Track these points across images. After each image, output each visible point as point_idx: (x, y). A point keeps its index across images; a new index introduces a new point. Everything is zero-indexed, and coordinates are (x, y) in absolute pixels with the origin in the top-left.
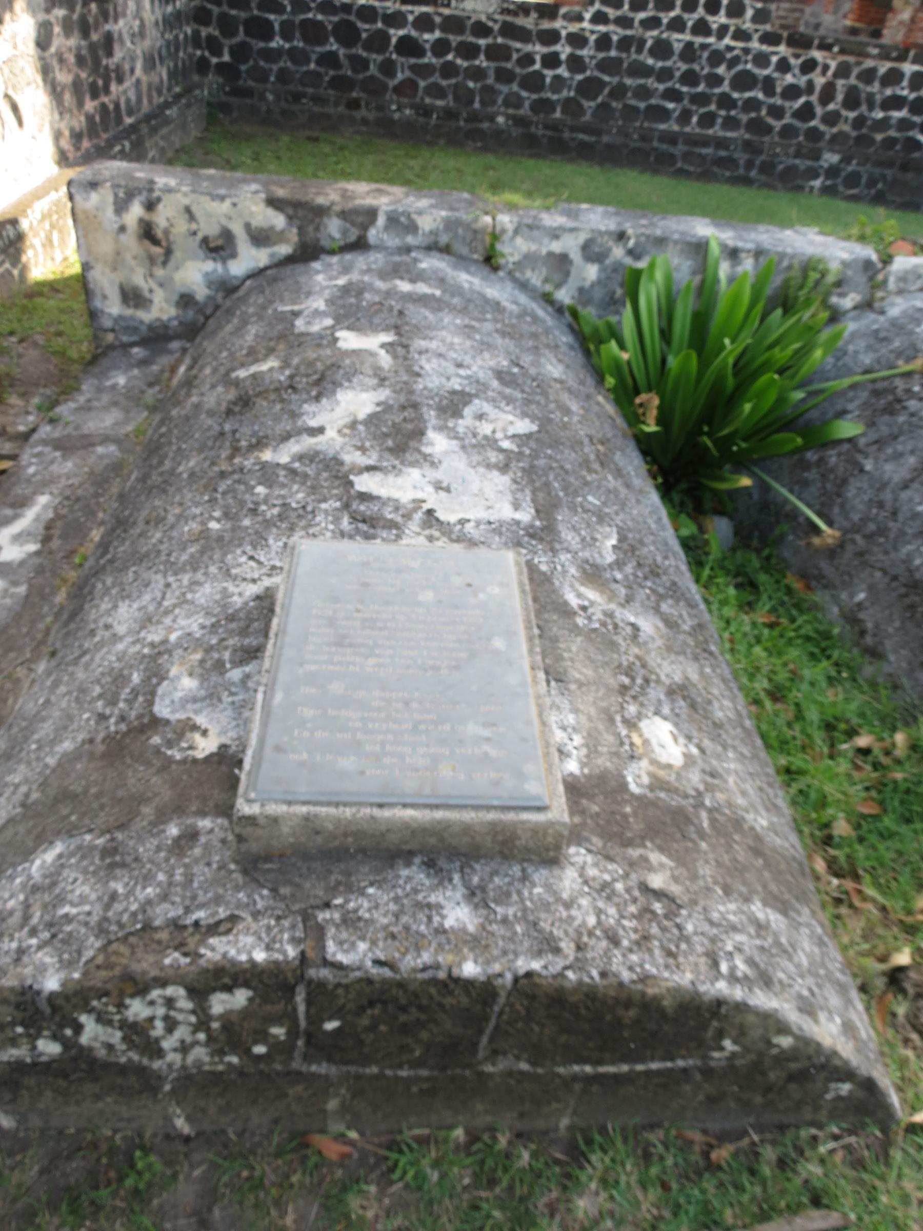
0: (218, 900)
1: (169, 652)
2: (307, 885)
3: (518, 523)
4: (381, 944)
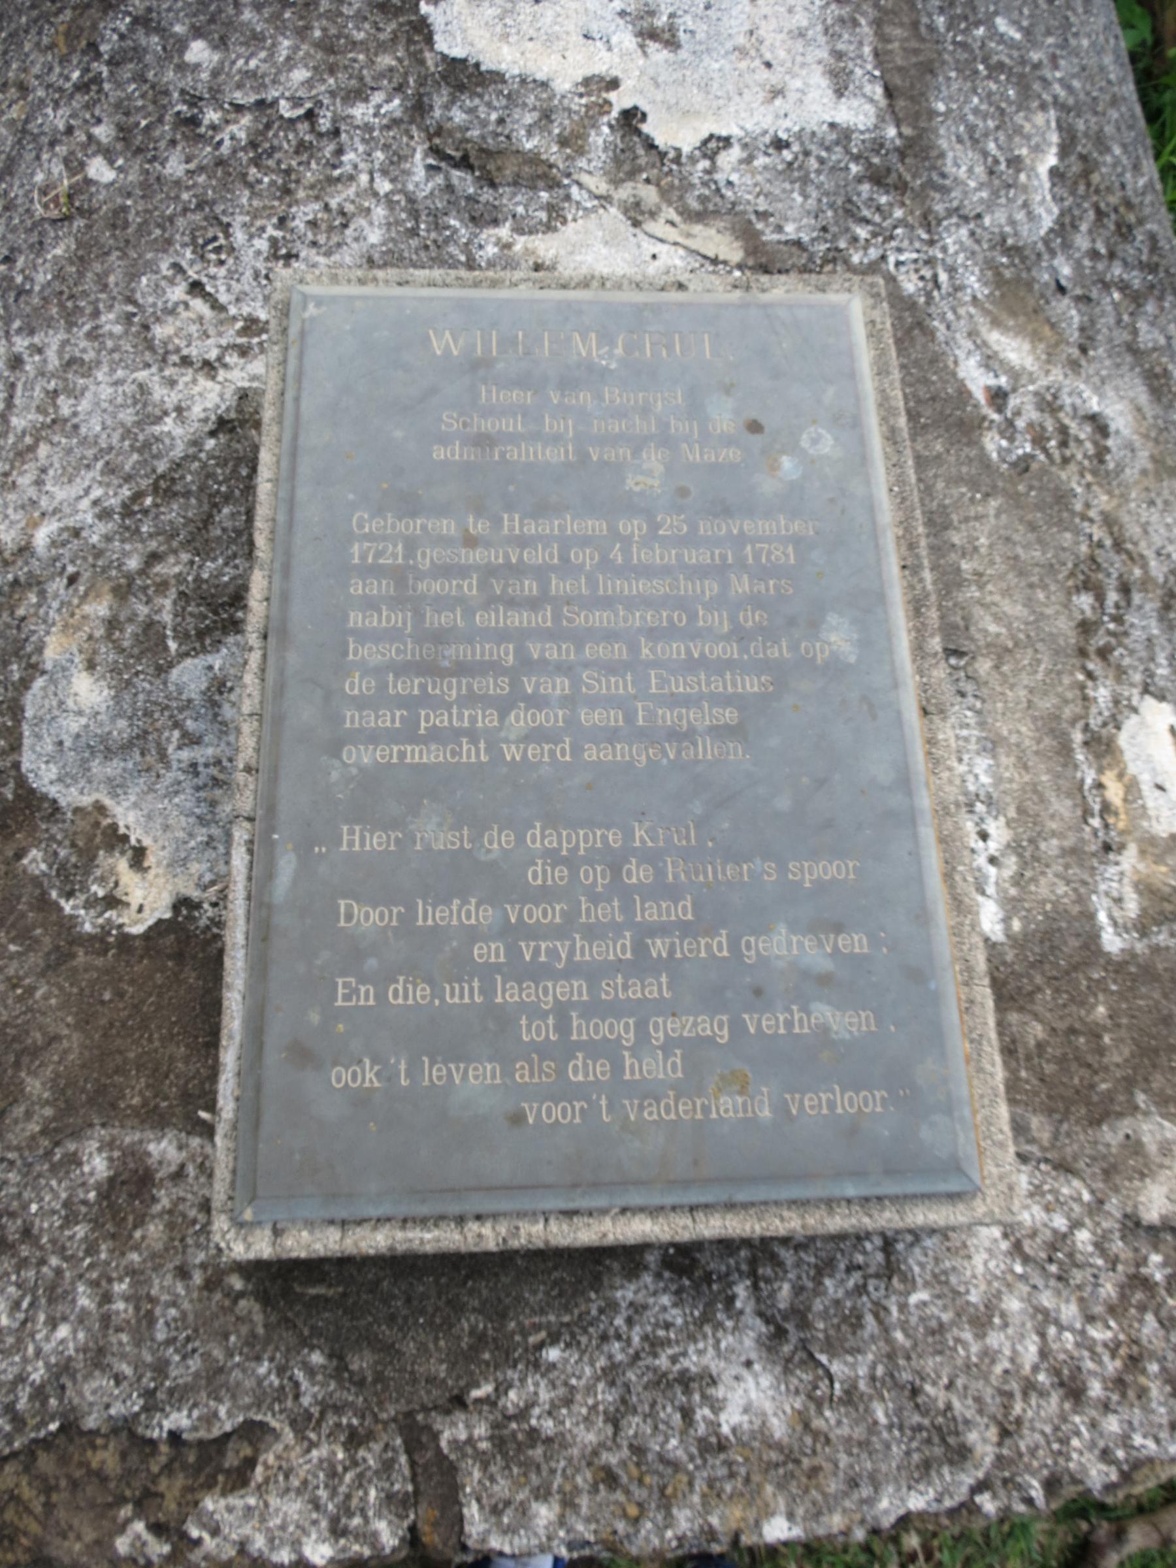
0: (214, 1379)
1: (36, 583)
2: (410, 1348)
3: (843, 134)
4: (584, 1502)
